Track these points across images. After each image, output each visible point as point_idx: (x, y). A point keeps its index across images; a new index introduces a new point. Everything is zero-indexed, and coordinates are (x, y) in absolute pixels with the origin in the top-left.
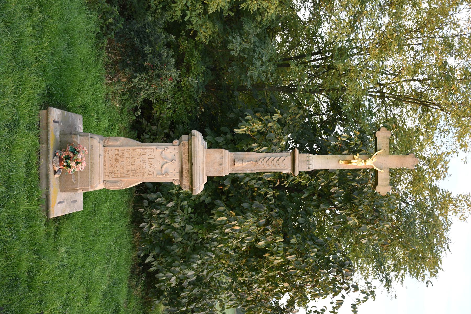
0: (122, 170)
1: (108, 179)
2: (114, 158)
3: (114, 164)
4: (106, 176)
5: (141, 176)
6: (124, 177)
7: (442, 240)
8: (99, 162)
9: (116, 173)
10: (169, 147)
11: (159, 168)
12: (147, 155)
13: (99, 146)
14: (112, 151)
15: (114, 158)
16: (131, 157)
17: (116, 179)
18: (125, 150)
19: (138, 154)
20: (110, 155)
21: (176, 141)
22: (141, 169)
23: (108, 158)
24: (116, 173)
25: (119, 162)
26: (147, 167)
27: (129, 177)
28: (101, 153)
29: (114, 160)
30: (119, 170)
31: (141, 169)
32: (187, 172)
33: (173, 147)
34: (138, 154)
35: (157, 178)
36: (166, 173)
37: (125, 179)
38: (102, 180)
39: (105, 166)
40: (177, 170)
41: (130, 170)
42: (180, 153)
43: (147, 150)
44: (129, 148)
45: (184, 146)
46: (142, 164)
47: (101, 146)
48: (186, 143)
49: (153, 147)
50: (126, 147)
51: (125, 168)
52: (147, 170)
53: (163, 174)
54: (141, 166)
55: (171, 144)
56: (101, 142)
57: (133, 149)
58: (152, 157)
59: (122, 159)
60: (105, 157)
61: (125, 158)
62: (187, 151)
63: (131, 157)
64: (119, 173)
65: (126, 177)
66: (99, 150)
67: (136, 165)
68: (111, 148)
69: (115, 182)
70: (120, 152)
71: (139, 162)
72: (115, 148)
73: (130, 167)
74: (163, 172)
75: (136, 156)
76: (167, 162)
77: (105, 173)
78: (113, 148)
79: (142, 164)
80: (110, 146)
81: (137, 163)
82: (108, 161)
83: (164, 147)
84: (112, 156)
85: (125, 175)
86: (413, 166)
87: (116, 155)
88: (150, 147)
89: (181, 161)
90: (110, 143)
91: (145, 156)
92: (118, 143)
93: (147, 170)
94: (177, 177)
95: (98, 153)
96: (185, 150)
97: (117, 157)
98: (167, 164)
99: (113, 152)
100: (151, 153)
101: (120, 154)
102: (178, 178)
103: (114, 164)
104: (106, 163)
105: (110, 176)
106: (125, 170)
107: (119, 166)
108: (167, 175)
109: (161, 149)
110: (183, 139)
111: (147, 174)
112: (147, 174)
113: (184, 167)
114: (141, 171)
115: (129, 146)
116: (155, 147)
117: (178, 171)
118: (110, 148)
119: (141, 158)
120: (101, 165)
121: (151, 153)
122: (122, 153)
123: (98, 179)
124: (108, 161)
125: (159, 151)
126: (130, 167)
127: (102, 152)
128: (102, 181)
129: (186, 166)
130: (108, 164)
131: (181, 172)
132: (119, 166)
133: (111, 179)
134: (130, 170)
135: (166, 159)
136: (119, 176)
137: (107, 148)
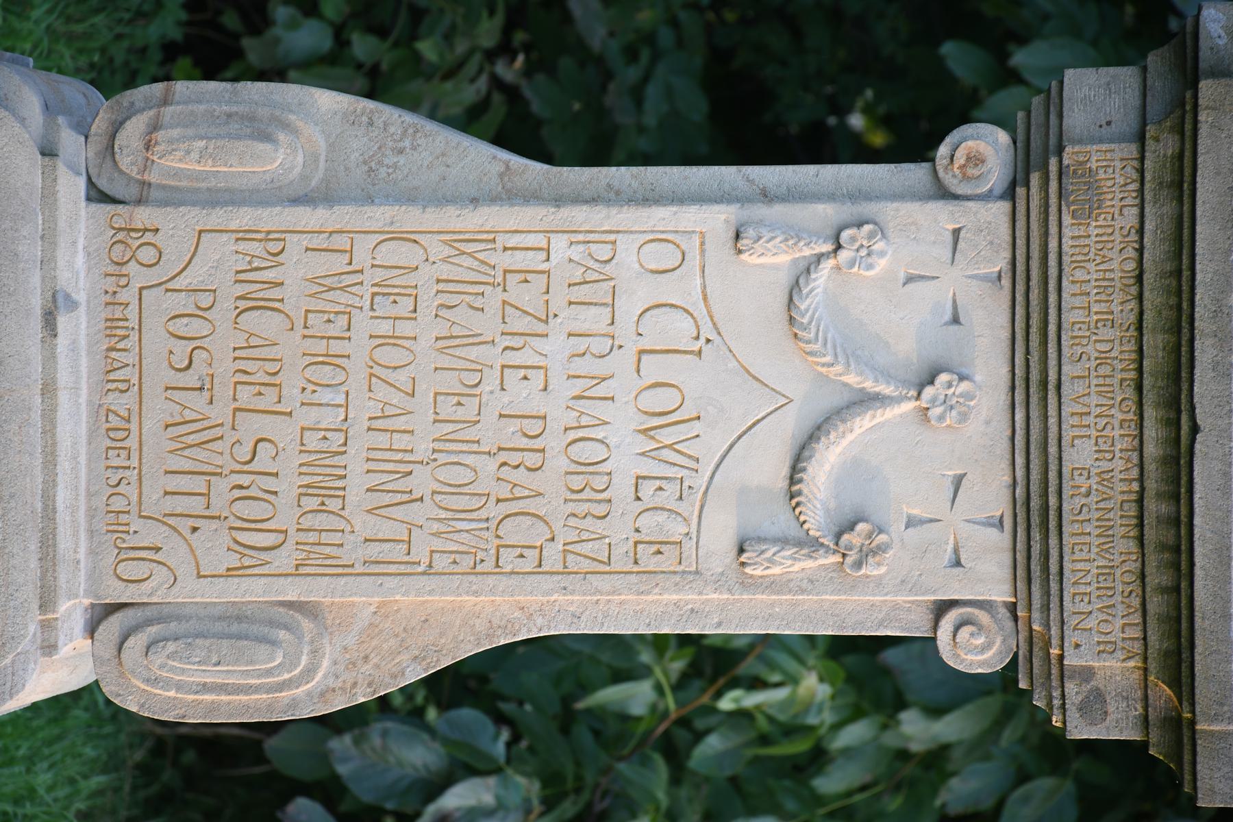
0: (323, 490)
1: (155, 591)
2: (224, 341)
3: (220, 412)
4: (129, 553)
5: (552, 553)
6: (345, 570)
7: (512, 205)
8: (49, 389)
9: (254, 526)
10: (890, 212)
11: (764, 465)
12: (629, 307)
13: (49, 196)
14: (199, 251)
15: (224, 341)
16: (427, 329)
17: (252, 591)
18: (362, 247)
19: (519, 294)
20: (181, 303)
21: (982, 148)
22: (552, 480)
23: (156, 340)
24: (254, 526)
25: (292, 393)
26: (625, 458)
27: (407, 570)
28: (64, 278)
29: (225, 367)
30: (288, 486)
31: (552, 480)
32: (1122, 527)
33: (943, 216)
34: (519, 294)
35: (749, 584)
36: (851, 534)
37: (361, 598)
38: (72, 610)
39: (114, 433)
40: (991, 492)
41: (421, 481)
42: (1033, 290)
43: (627, 248)
44: (411, 218)
45: (1089, 211)
46: (560, 416)
47: (71, 187)
48: (1106, 165)
49: (691, 217)
50: (379, 215)
51: (355, 463)
52: (622, 489)
53: (811, 545)
54: (554, 442)
55: (913, 174)
56: (69, 140)
57: (457, 241)
58: (679, 330)
59: (327, 360)
60: (115, 329)
61: (358, 348)
62: (1121, 264)
63: (427, 329)
64: (286, 518)
65: (376, 569)
66: (49, 237)
67: (490, 433)
68: (194, 217)
69: (239, 627)
70: (297, 269)
71: (523, 395)
72: (243, 218)
73: (423, 449)
74: (816, 519)
75: (487, 324)
76: (865, 401)
77: (112, 525)
78: (217, 218)
79: (560, 416)
80: (174, 198)
81: (497, 403)
82: (159, 375)
83: (826, 213)
84: (201, 313)
85: (353, 553)
86: (1001, 288)
87: (250, 305)
88: (661, 217)
89: (1034, 382)
90: (181, 159)
91: (594, 319)
92: (277, 161)
93: (622, 489)
94: (990, 577)
95: (36, 279)
96: (1100, 250)
97: (264, 324)
98: (863, 423)
99: (218, 262)
100: (667, 290)
101: (294, 297)
102: (1000, 594)
103: (220, 412)
104: (122, 403)
105: (174, 552)
106: (357, 483)
107: (283, 432)
108: (868, 553)
109: (795, 234)
110: (1076, 118)
111: (619, 531)
112: (619, 531)
113: (1080, 455)
114: (554, 506)
115: (410, 197)
116: (716, 220)
117: (999, 504)
118: (174, 226)
119: (556, 347)
120: (74, 425)
121: (667, 290)
122: (322, 286)
123: (29, 594)
124: (159, 375)
125: (773, 259)
126: (423, 449)
127: (77, 268)
128: (78, 622)
129: (1099, 447)
130: (158, 410)
131: (1036, 517)
132: (283, 432)
133: (193, 593)
134: (421, 481)
135: (851, 354)
136: (284, 559)
137: (143, 216)
